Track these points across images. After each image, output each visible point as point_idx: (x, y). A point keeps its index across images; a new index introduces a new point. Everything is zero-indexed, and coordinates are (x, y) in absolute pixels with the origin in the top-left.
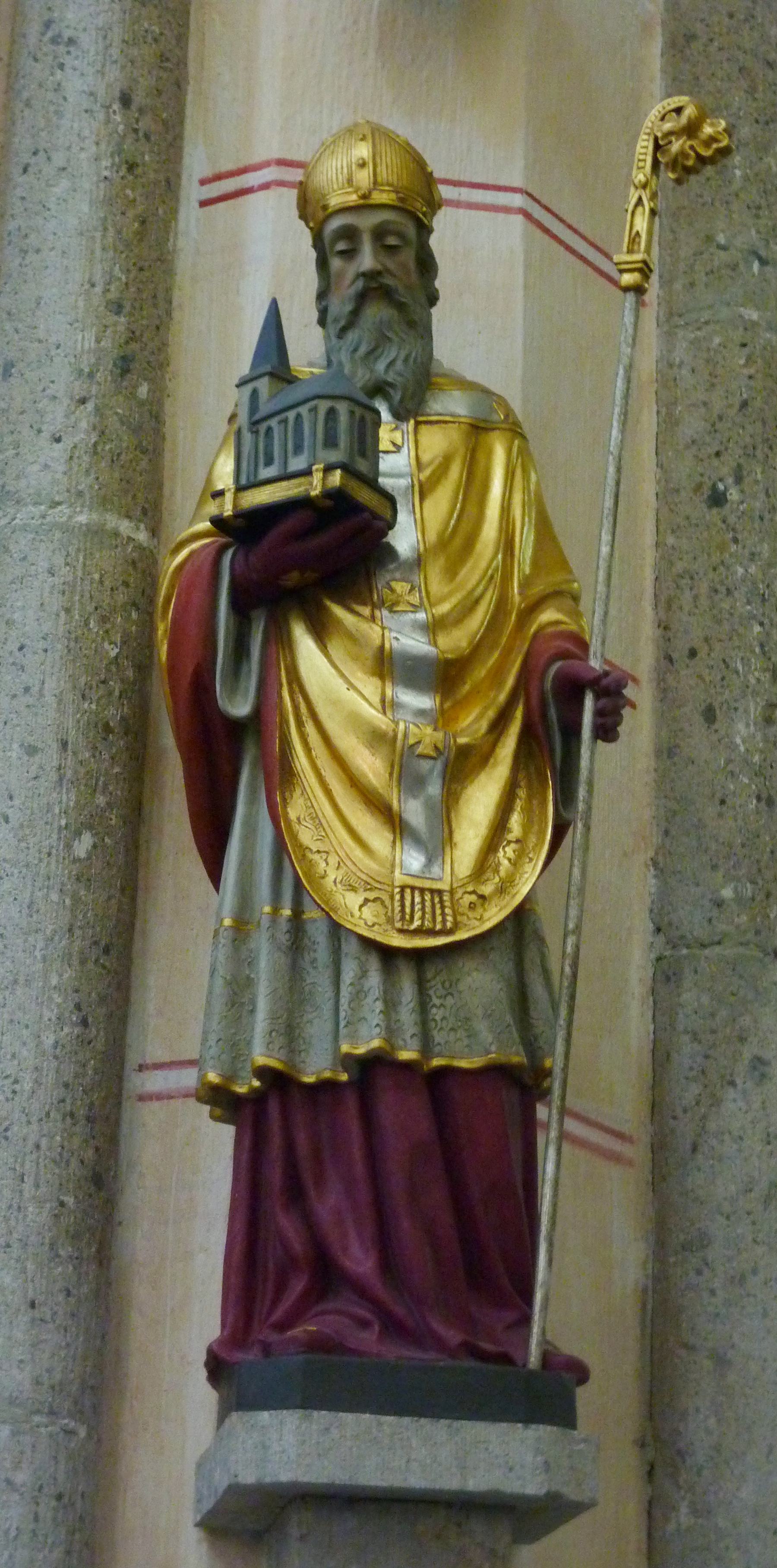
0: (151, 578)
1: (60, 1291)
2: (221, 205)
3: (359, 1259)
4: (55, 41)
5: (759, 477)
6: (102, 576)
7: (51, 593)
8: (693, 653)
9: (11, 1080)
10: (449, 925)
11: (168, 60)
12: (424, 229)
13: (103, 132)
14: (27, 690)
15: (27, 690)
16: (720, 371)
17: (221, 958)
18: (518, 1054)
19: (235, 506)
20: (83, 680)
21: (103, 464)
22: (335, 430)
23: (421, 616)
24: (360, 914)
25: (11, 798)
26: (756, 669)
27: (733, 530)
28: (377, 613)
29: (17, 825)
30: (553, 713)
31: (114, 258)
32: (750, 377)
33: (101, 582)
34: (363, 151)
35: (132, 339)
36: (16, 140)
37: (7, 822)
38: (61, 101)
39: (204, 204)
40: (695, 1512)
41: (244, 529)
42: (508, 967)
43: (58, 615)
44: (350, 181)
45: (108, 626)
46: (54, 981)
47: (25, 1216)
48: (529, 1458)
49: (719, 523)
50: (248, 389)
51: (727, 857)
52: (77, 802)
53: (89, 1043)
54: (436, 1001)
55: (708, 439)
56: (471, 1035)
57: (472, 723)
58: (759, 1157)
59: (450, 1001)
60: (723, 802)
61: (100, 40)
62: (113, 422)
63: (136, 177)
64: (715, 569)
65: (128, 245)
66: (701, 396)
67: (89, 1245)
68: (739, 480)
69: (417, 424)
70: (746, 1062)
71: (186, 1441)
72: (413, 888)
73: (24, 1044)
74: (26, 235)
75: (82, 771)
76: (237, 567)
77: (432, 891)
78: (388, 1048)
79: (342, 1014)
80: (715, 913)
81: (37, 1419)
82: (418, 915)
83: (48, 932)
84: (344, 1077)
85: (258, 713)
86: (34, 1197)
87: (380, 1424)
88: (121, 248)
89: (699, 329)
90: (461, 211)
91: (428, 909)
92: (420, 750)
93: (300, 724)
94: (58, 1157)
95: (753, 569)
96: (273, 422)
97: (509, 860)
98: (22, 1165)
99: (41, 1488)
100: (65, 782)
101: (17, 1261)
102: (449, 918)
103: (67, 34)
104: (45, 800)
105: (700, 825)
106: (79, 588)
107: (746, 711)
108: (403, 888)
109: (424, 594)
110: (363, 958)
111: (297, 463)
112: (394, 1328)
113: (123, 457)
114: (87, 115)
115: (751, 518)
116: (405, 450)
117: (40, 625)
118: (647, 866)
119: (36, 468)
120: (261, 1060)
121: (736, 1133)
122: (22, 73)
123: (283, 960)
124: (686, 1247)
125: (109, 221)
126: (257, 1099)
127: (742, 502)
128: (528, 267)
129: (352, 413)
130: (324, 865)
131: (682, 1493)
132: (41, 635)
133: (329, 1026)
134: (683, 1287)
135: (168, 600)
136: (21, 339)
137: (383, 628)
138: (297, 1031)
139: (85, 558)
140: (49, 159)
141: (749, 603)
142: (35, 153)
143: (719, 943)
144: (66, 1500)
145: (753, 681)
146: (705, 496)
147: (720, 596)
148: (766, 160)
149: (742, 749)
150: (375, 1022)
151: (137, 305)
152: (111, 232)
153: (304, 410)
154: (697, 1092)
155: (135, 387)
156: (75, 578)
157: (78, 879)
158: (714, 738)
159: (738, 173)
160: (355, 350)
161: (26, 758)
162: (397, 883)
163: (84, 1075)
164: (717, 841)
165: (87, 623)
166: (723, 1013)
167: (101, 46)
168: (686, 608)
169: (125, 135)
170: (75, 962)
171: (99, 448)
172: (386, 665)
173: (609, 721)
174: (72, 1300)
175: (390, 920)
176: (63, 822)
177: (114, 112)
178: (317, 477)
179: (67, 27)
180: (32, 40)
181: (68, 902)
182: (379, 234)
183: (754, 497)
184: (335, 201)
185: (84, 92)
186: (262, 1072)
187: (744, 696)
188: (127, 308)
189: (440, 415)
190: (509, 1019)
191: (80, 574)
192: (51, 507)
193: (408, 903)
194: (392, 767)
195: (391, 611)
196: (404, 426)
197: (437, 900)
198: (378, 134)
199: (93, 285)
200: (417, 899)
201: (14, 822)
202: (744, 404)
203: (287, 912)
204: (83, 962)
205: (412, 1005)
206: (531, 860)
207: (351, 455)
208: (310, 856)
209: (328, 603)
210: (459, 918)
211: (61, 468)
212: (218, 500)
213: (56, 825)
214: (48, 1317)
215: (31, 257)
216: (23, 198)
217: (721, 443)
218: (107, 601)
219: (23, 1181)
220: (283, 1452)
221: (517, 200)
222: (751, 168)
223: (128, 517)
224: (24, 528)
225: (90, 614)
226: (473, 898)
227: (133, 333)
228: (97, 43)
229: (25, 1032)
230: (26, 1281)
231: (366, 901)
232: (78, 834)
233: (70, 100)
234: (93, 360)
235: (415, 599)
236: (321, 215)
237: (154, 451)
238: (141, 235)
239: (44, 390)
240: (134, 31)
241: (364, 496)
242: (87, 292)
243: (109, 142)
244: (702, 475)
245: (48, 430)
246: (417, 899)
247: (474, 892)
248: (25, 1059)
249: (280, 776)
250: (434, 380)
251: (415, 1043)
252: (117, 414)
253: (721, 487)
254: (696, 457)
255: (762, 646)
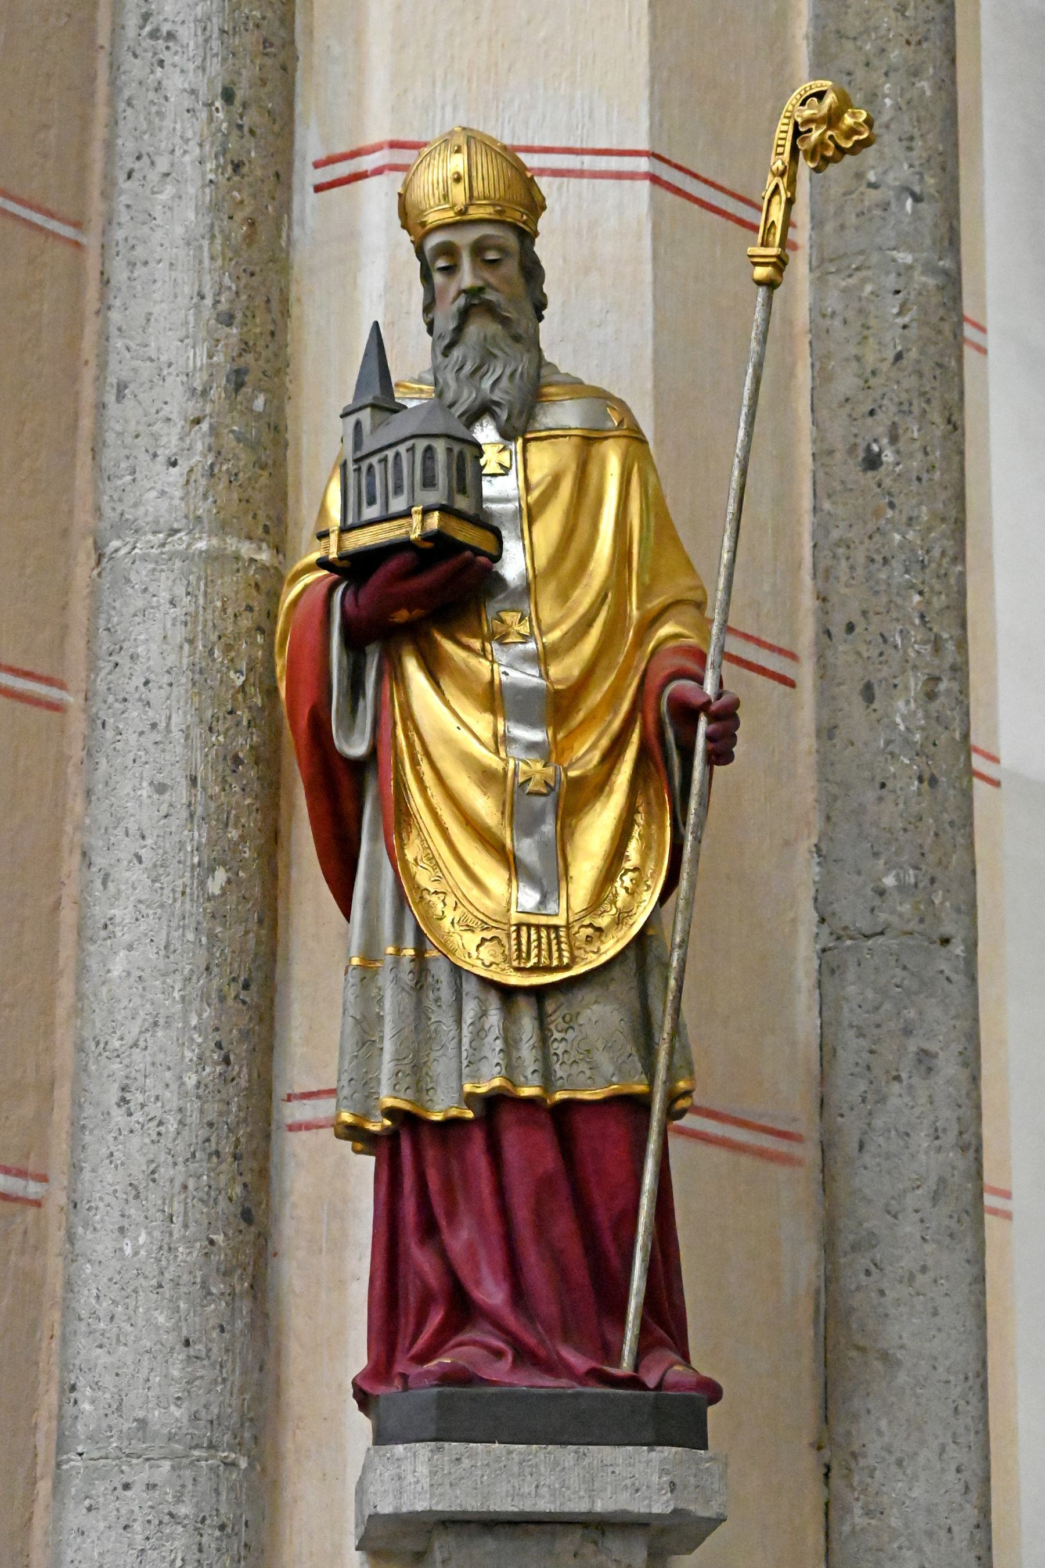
0: (275, 596)
1: (214, 1328)
2: (335, 191)
3: (491, 1292)
4: (154, 35)
5: (916, 435)
6: (224, 602)
7: (174, 625)
8: (850, 628)
9: (155, 1122)
10: (566, 960)
11: (272, 45)
12: (527, 236)
13: (206, 132)
14: (154, 726)
15: (154, 726)
16: (872, 322)
17: (351, 998)
18: (640, 1083)
19: (339, 548)
20: (209, 713)
21: (221, 487)
22: (433, 469)
23: (531, 646)
24: (477, 955)
25: (143, 837)
26: (915, 642)
27: (889, 494)
28: (488, 646)
29: (150, 866)
30: (670, 735)
31: (222, 267)
32: (905, 327)
33: (224, 610)
34: (458, 163)
35: (245, 350)
36: (120, 142)
37: (140, 862)
38: (162, 101)
39: (318, 188)
40: (868, 1513)
41: (354, 568)
42: (632, 997)
43: (181, 648)
44: (446, 196)
45: (233, 654)
46: (194, 1021)
47: (176, 1257)
48: (655, 1478)
49: (875, 487)
50: (352, 420)
51: (888, 843)
52: (209, 839)
53: (233, 1080)
54: (557, 1035)
55: (861, 397)
56: (592, 1064)
57: (586, 753)
58: (927, 1153)
59: (570, 1035)
60: (883, 786)
61: (199, 33)
62: (229, 441)
63: (243, 177)
64: (870, 537)
65: (237, 252)
66: (852, 350)
67: (241, 1279)
68: (894, 439)
69: (526, 442)
70: (911, 1056)
71: (346, 1469)
72: (529, 926)
73: (167, 1085)
74: (133, 247)
75: (213, 805)
76: (347, 605)
77: (548, 927)
78: (509, 1086)
79: (464, 1054)
80: (877, 902)
81: (196, 1453)
82: (534, 952)
83: (186, 972)
84: (470, 1115)
85: (373, 752)
86: (184, 1237)
87: (510, 1452)
88: (230, 255)
89: (850, 276)
90: (585, 181)
91: (544, 946)
92: (531, 787)
93: (415, 763)
94: (205, 1197)
95: (911, 535)
96: (374, 460)
97: (626, 889)
98: (171, 1206)
99: (204, 1519)
100: (196, 819)
101: (170, 1301)
102: (566, 954)
103: (165, 28)
104: (177, 838)
105: (862, 809)
106: (201, 618)
107: (907, 688)
108: (519, 926)
109: (534, 623)
110: (482, 997)
111: (398, 504)
112: (526, 1356)
113: (241, 475)
114: (187, 115)
115: (909, 480)
116: (513, 471)
117: (164, 658)
118: (810, 852)
119: (153, 494)
120: (389, 1102)
121: (902, 1130)
122: (122, 69)
123: (408, 1001)
124: (855, 1247)
125: (216, 228)
126: (391, 1137)
127: (898, 464)
128: (656, 237)
129: (449, 450)
130: (440, 905)
131: (856, 1494)
132: (165, 669)
133: (453, 1064)
134: (853, 1288)
135: (284, 638)
136: (132, 358)
137: (493, 662)
138: (424, 1070)
139: (206, 585)
140: (153, 163)
141: (907, 572)
142: (139, 158)
143: (882, 933)
144: (229, 1530)
145: (912, 654)
146: (860, 459)
147: (876, 566)
148: (918, 85)
149: (902, 727)
150: (496, 1061)
151: (249, 313)
152: (219, 240)
153: (402, 449)
154: (863, 1088)
155: (251, 400)
156: (197, 607)
157: (213, 917)
158: (874, 716)
159: (888, 102)
160: (461, 368)
161: (156, 796)
162: (513, 922)
163: (229, 1112)
164: (878, 826)
165: (211, 652)
166: (888, 1006)
167: (200, 39)
168: (843, 579)
169: (229, 134)
170: (215, 1000)
171: (216, 471)
172: (494, 698)
173: (718, 746)
174: (227, 1336)
175: (507, 959)
176: (196, 860)
177: (217, 110)
178: (417, 519)
179: (166, 20)
180: (131, 31)
181: (204, 940)
182: (478, 249)
183: (911, 456)
184: (433, 218)
185: (185, 90)
186: (390, 1113)
187: (903, 672)
188: (239, 316)
189: (551, 429)
190: (630, 1048)
191: (201, 601)
192: (170, 535)
193: (524, 940)
194: (504, 804)
195: (502, 644)
196: (512, 447)
197: (553, 936)
198: (473, 140)
199: (203, 297)
200: (534, 937)
201: (147, 863)
202: (899, 357)
203: (410, 952)
204: (222, 999)
205: (531, 1042)
206: (649, 887)
207: (450, 497)
208: (427, 897)
209: (438, 637)
210: (576, 953)
211: (178, 493)
212: (324, 541)
213: (189, 863)
214: (203, 1354)
215: (139, 271)
216: (128, 206)
217: (875, 401)
218: (230, 629)
219: (172, 1221)
220: (418, 1482)
221: (643, 164)
222: (901, 96)
223: (249, 538)
224: (144, 558)
225: (214, 644)
226: (590, 931)
227: (246, 344)
228: (196, 35)
229: (168, 1074)
230: (180, 1320)
231: (483, 940)
232: (212, 870)
233: (172, 100)
234: (205, 377)
235: (525, 629)
236: (420, 231)
237: (274, 464)
238: (250, 239)
239: (157, 412)
240: (234, 19)
241: (466, 534)
242: (197, 306)
243: (213, 143)
244: (856, 436)
245: (163, 454)
246: (534, 937)
247: (591, 925)
248: (169, 1101)
249: (399, 819)
250: (546, 390)
251: (536, 1079)
252: (233, 431)
253: (875, 448)
254: (850, 416)
255: (922, 617)
